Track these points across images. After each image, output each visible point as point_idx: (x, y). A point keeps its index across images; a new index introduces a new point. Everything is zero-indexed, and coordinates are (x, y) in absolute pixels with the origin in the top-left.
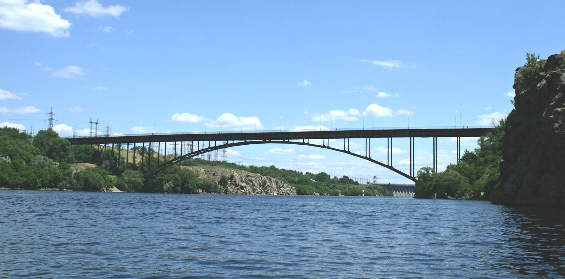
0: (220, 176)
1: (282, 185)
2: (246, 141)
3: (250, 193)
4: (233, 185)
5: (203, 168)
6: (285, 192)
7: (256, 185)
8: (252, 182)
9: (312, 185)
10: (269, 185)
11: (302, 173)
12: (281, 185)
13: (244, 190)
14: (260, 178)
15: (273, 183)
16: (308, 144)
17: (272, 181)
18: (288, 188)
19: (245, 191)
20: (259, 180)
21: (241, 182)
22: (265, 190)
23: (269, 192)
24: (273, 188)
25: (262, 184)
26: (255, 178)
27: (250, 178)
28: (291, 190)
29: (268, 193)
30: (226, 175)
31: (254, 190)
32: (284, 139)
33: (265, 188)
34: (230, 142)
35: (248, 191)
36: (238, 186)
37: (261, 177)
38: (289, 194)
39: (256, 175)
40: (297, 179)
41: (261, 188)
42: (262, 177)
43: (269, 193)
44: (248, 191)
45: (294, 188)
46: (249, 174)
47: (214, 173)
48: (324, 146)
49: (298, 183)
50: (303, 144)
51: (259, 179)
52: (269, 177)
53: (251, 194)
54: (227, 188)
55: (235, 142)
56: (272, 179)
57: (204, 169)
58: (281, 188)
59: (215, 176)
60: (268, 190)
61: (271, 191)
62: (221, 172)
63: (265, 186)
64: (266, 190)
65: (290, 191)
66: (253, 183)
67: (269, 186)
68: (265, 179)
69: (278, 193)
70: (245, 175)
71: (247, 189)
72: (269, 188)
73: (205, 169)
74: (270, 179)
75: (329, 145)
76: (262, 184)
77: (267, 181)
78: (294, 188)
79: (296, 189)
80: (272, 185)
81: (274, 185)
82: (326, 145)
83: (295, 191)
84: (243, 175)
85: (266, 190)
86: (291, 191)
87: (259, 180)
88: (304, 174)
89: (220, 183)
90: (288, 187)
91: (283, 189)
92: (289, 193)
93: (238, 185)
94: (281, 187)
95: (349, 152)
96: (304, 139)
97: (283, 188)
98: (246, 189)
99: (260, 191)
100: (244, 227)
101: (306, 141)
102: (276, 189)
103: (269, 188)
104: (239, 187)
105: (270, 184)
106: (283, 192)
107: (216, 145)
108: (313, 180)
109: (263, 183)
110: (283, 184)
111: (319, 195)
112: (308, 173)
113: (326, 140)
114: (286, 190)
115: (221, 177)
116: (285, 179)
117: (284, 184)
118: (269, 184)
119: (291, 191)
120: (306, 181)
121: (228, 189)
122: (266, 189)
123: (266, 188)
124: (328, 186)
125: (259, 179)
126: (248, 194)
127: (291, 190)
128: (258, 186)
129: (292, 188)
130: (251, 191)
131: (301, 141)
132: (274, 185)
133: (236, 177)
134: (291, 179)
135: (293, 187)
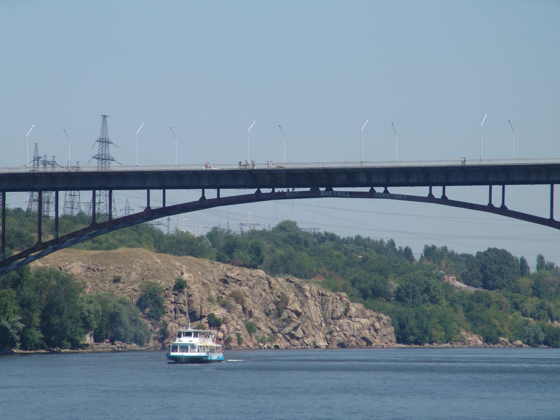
0: (136, 286)
1: (342, 310)
2: (258, 192)
3: (240, 341)
4: (185, 313)
5: (80, 260)
6: (356, 333)
7: (257, 313)
8: (242, 302)
9: (452, 303)
10: (300, 310)
11: (408, 252)
12: (340, 310)
13: (223, 332)
14: (267, 287)
15: (311, 302)
16: (444, 200)
17: (306, 296)
18: (364, 321)
19: (224, 337)
20: (264, 294)
21: (208, 304)
22: (284, 327)
23: (299, 333)
24: (310, 319)
25: (272, 307)
26: (250, 287)
27: (234, 287)
28: (377, 325)
29: (293, 336)
30: (159, 282)
31: (251, 329)
32: (372, 185)
33: (284, 320)
34: (211, 194)
35: (233, 336)
36: (202, 317)
37: (270, 283)
38: (369, 343)
39: (251, 275)
40: (393, 285)
41: (272, 323)
42: (273, 280)
43: (298, 339)
44: (233, 336)
45: (384, 317)
46: (229, 274)
47: (117, 274)
48: (490, 208)
49: (400, 297)
50: (430, 199)
51: (265, 290)
52: (297, 280)
53: (244, 345)
54: (165, 324)
55: (226, 193)
56: (307, 287)
57: (80, 263)
58: (341, 321)
59: (121, 285)
60: (295, 329)
61: (304, 333)
62: (139, 270)
63: (285, 315)
64: (287, 330)
65: (372, 331)
66: (246, 305)
67: (298, 314)
68: (281, 286)
69: (328, 337)
70: (217, 279)
71: (231, 329)
72: (299, 321)
73: (84, 262)
74: (299, 288)
75: (506, 204)
76: (274, 307)
77: (291, 296)
78: (385, 318)
79: (393, 325)
80: (306, 310)
81: (313, 308)
82: (497, 204)
83: (391, 329)
84: (211, 278)
85: (287, 330)
86: (376, 330)
87: (264, 294)
88: (418, 253)
89: (141, 304)
90: (365, 317)
91: (349, 325)
92: (368, 336)
93: (198, 314)
94: (339, 318)
95: (553, 220)
96: (431, 184)
97: (346, 320)
98: (228, 328)
99: (269, 331)
100: (386, 377)
101: (437, 191)
102: (324, 325)
103: (299, 321)
104: (205, 320)
105: (302, 305)
106: (348, 333)
107: (167, 205)
108: (458, 284)
109: (276, 303)
110: (348, 305)
111: (480, 342)
112: (434, 247)
113: (497, 189)
114: (358, 326)
115: (140, 286)
116: (349, 283)
117: (351, 304)
118: (296, 306)
119: (376, 330)
120: (427, 290)
121: (168, 328)
122: (289, 323)
123: (289, 320)
124: (516, 307)
125: (265, 290)
126: (234, 344)
127: (373, 326)
128: (262, 316)
129: (379, 319)
130: (244, 333)
131: (422, 191)
132: (313, 308)
133: (193, 287)
134: (371, 283)
135: (382, 315)
